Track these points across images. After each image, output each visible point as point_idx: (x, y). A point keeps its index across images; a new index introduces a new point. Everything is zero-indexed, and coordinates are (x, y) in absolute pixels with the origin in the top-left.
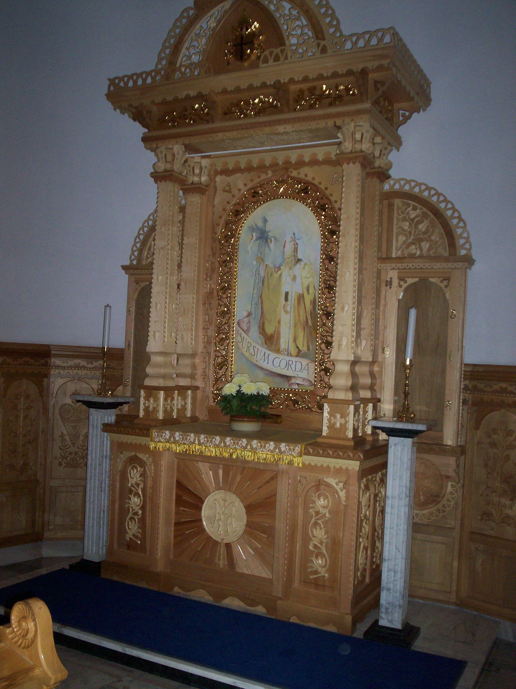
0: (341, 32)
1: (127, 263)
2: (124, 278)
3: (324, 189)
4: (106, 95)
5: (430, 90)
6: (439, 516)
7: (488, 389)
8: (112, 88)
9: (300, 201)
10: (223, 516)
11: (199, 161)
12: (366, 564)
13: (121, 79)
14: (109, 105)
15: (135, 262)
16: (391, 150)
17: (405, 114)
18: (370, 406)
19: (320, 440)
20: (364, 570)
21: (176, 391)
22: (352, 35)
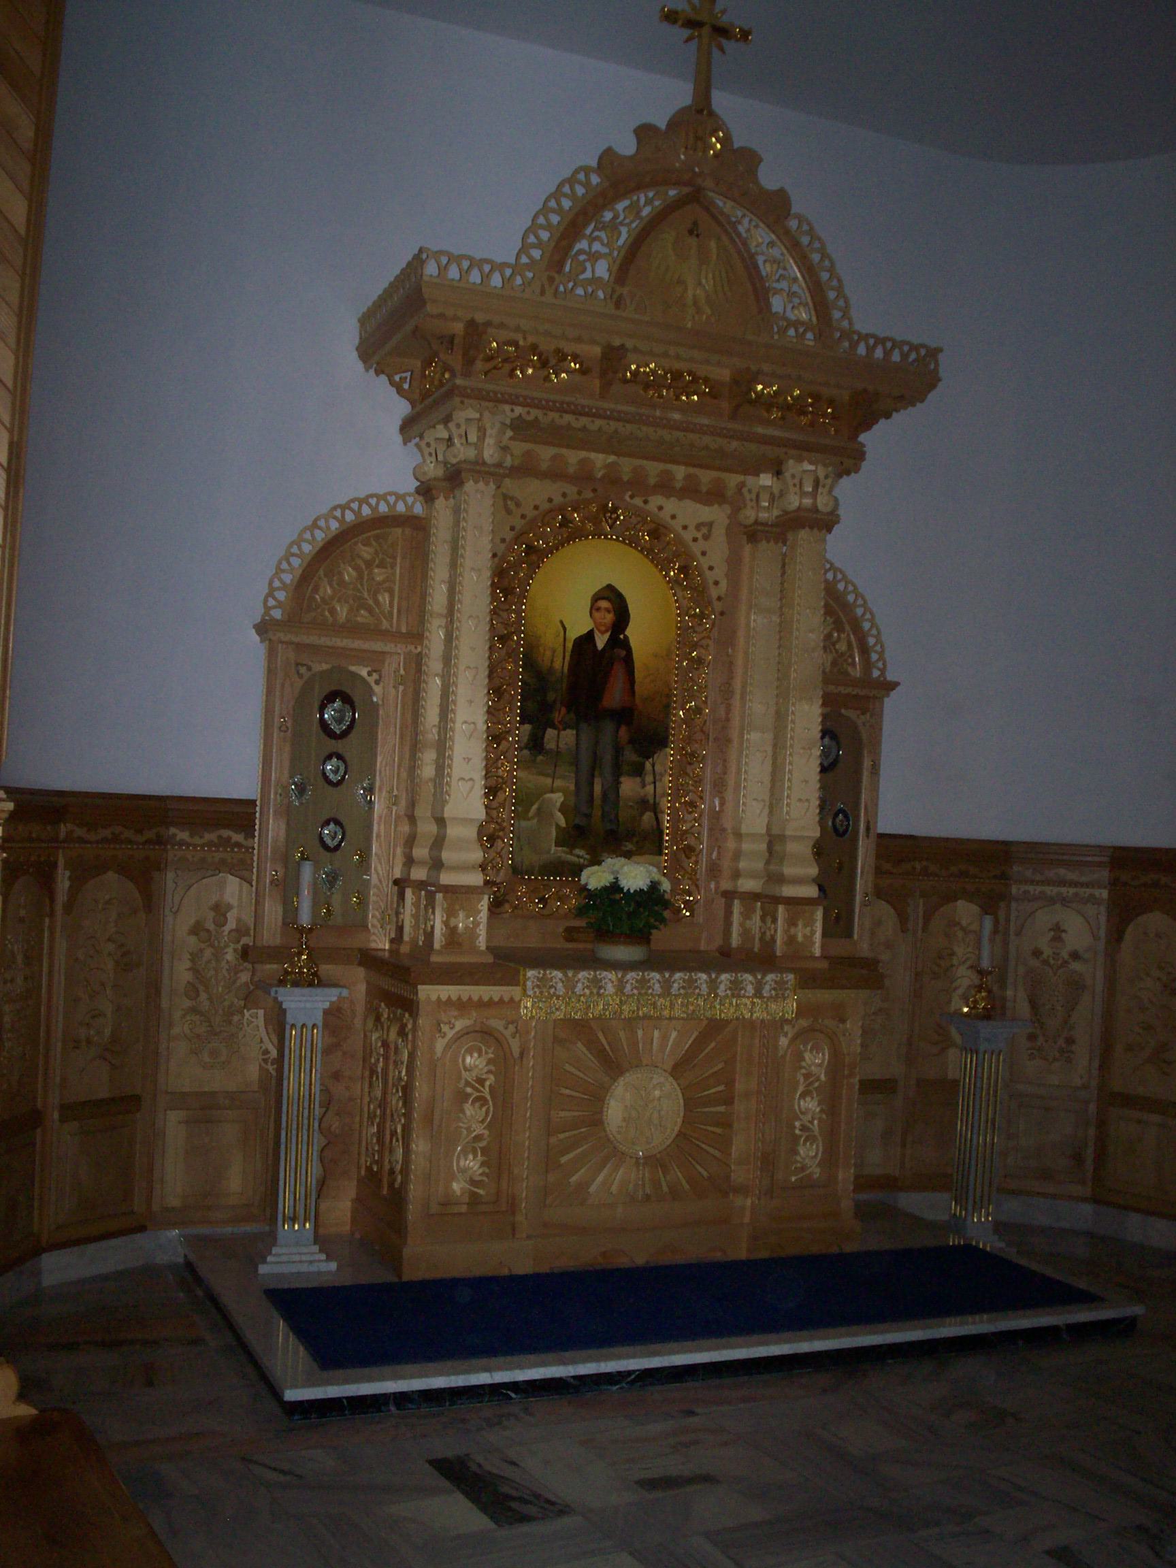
7: (1038, 877)
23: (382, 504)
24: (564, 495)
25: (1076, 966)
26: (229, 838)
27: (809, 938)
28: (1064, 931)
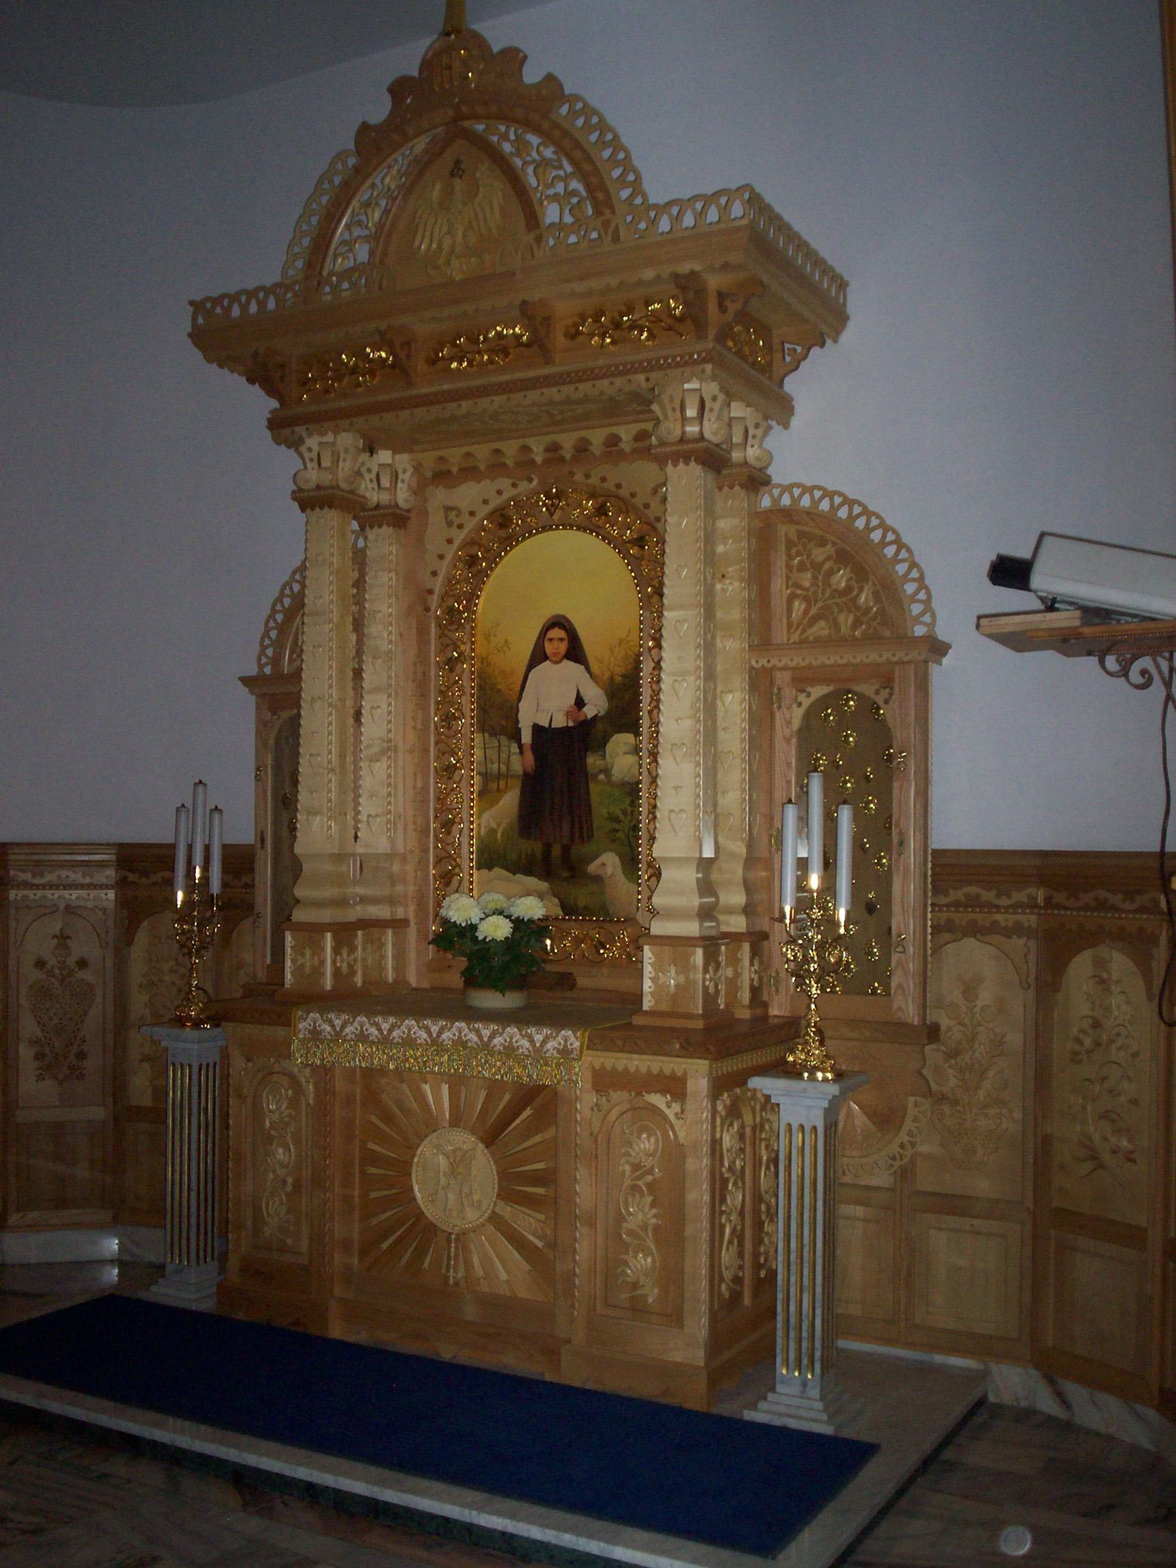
0: (645, 196)
1: (253, 671)
2: (247, 701)
3: (641, 506)
4: (190, 335)
5: (845, 299)
6: (892, 1166)
7: (37, 881)
8: (200, 320)
9: (591, 533)
10: (453, 1181)
11: (389, 461)
12: (741, 1267)
13: (217, 301)
14: (197, 354)
15: (268, 670)
16: (770, 428)
17: (795, 350)
18: (746, 947)
19: (637, 1020)
20: (737, 1280)
21: (360, 933)
22: (669, 204)
23: (807, 497)
24: (499, 492)
25: (81, 975)
26: (978, 896)
27: (659, 967)
28: (68, 937)
